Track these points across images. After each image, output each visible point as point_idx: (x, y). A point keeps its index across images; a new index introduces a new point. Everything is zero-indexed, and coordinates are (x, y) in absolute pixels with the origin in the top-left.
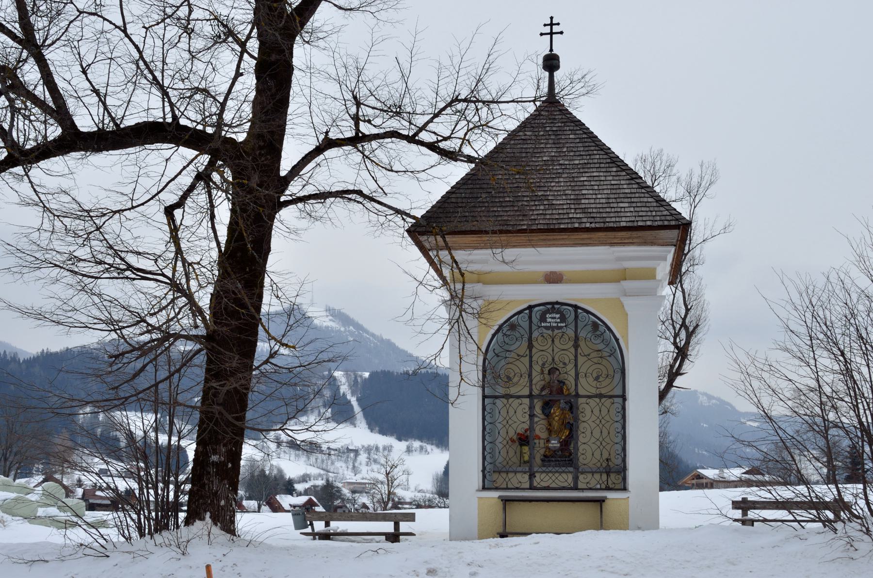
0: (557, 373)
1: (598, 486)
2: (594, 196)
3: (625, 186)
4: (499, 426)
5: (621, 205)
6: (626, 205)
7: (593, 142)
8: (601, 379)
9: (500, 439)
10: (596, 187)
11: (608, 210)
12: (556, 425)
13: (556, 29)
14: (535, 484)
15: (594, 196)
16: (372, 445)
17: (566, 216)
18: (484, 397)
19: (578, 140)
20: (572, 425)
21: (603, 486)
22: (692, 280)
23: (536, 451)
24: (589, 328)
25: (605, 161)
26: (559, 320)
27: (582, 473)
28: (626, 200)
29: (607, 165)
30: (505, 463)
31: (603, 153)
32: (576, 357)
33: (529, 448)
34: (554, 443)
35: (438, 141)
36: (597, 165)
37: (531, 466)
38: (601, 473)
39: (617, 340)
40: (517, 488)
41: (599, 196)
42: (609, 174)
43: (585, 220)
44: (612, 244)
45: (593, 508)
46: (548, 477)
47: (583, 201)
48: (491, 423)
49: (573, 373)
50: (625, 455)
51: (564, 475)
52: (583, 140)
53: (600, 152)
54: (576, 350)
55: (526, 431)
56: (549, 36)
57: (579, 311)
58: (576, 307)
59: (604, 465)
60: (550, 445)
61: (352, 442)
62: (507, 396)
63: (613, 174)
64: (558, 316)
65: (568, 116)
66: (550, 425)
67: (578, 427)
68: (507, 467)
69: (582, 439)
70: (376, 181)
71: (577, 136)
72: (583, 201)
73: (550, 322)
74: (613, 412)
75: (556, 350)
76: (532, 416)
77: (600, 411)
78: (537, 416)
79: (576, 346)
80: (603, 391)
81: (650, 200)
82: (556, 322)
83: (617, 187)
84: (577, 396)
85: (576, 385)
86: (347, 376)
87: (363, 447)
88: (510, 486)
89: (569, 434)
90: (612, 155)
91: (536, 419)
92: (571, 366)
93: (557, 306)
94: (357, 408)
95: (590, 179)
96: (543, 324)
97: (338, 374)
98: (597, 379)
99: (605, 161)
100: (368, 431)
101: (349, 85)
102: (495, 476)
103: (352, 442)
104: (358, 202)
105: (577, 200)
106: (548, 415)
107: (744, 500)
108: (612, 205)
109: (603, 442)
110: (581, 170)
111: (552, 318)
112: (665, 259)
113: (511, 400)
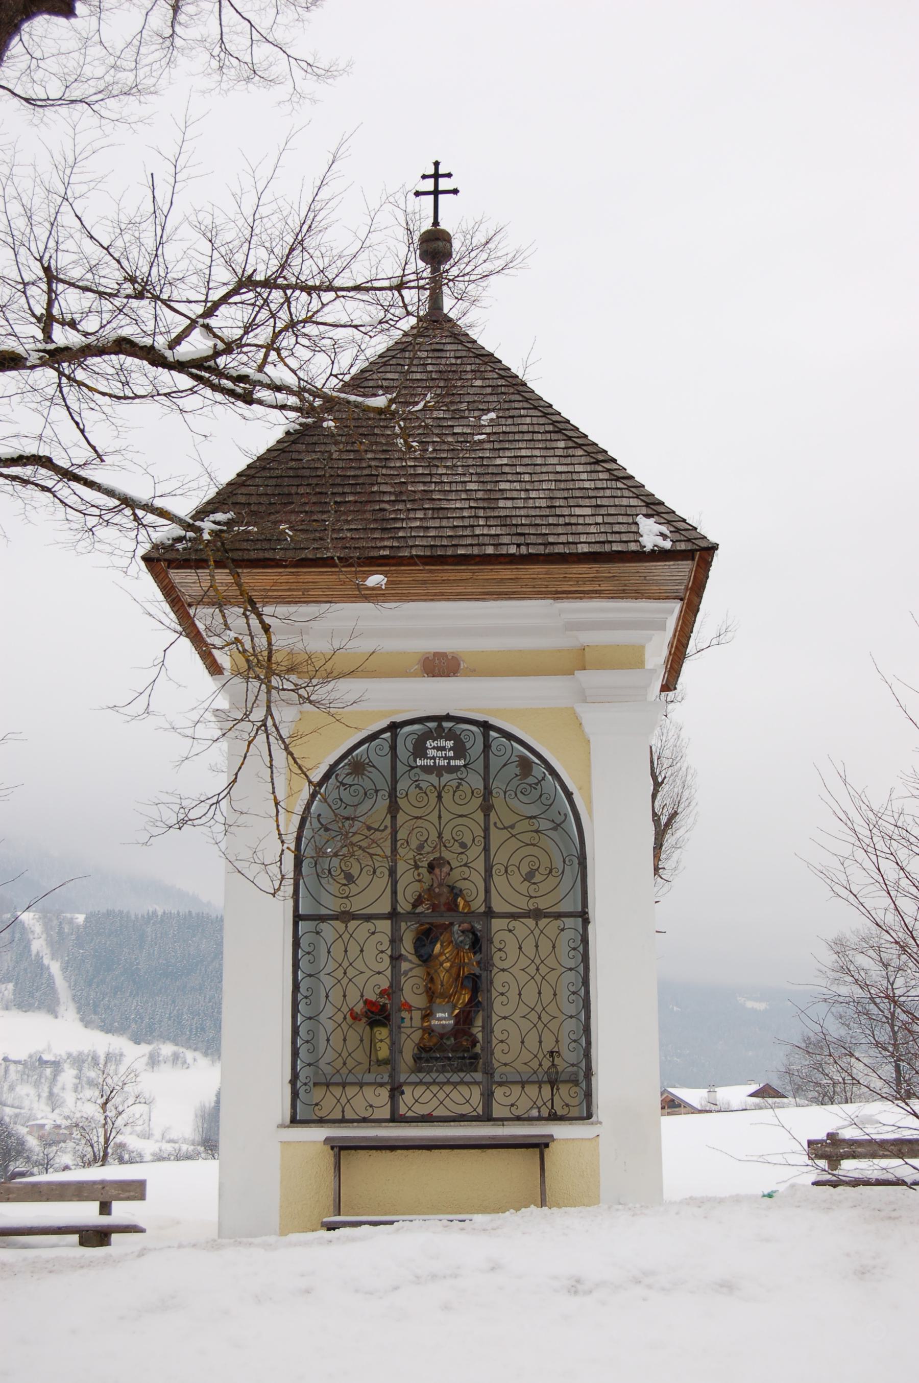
0: (446, 869)
1: (535, 1113)
2: (523, 495)
3: (584, 476)
4: (328, 982)
5: (578, 511)
6: (588, 511)
7: (519, 393)
8: (538, 878)
9: (329, 1011)
10: (527, 478)
11: (551, 520)
12: (443, 977)
13: (444, 184)
14: (403, 1110)
15: (523, 495)
16: (86, 1052)
17: (468, 532)
18: (297, 918)
19: (489, 390)
20: (479, 977)
21: (545, 1113)
22: (665, 731)
23: (404, 1037)
24: (514, 769)
25: (542, 429)
26: (451, 754)
27: (501, 1084)
28: (587, 502)
29: (548, 436)
30: (339, 1064)
31: (540, 414)
32: (486, 830)
33: (391, 1031)
34: (443, 1019)
35: (217, 354)
36: (528, 437)
37: (393, 1069)
38: (540, 1083)
39: (569, 795)
40: (365, 1120)
41: (533, 494)
42: (551, 452)
43: (506, 540)
44: (558, 595)
45: (524, 1161)
46: (428, 1095)
47: (501, 504)
48: (310, 976)
49: (480, 865)
50: (589, 1043)
51: (464, 1090)
52: (500, 390)
53: (531, 412)
54: (487, 816)
55: (383, 993)
56: (432, 197)
57: (493, 734)
58: (486, 726)
59: (547, 1064)
60: (434, 1022)
61: (49, 1046)
62: (345, 916)
63: (559, 452)
64: (450, 744)
65: (469, 345)
66: (432, 980)
67: (492, 982)
68: (344, 1071)
69: (499, 1008)
70: (82, 431)
71: (487, 382)
72: (501, 504)
73: (434, 758)
74: (563, 948)
75: (446, 816)
76: (396, 959)
77: (537, 946)
78: (406, 960)
79: (487, 808)
80: (543, 904)
81: (634, 502)
82: (445, 758)
83: (569, 477)
84: (490, 913)
85: (487, 891)
86: (47, 927)
87: (69, 1055)
88: (349, 1115)
89: (470, 1000)
90: (555, 418)
91: (405, 966)
92: (475, 851)
93: (447, 725)
94: (60, 983)
95: (515, 461)
96: (419, 762)
97: (27, 918)
98: (529, 877)
99: (542, 429)
100: (78, 1026)
101: (34, 249)
102: (318, 1094)
103: (49, 1046)
104: (45, 489)
105: (490, 501)
106: (425, 958)
107: (833, 1138)
108: (558, 511)
109: (544, 1015)
110: (497, 446)
111: (439, 749)
112: (663, 628)
113: (353, 924)
